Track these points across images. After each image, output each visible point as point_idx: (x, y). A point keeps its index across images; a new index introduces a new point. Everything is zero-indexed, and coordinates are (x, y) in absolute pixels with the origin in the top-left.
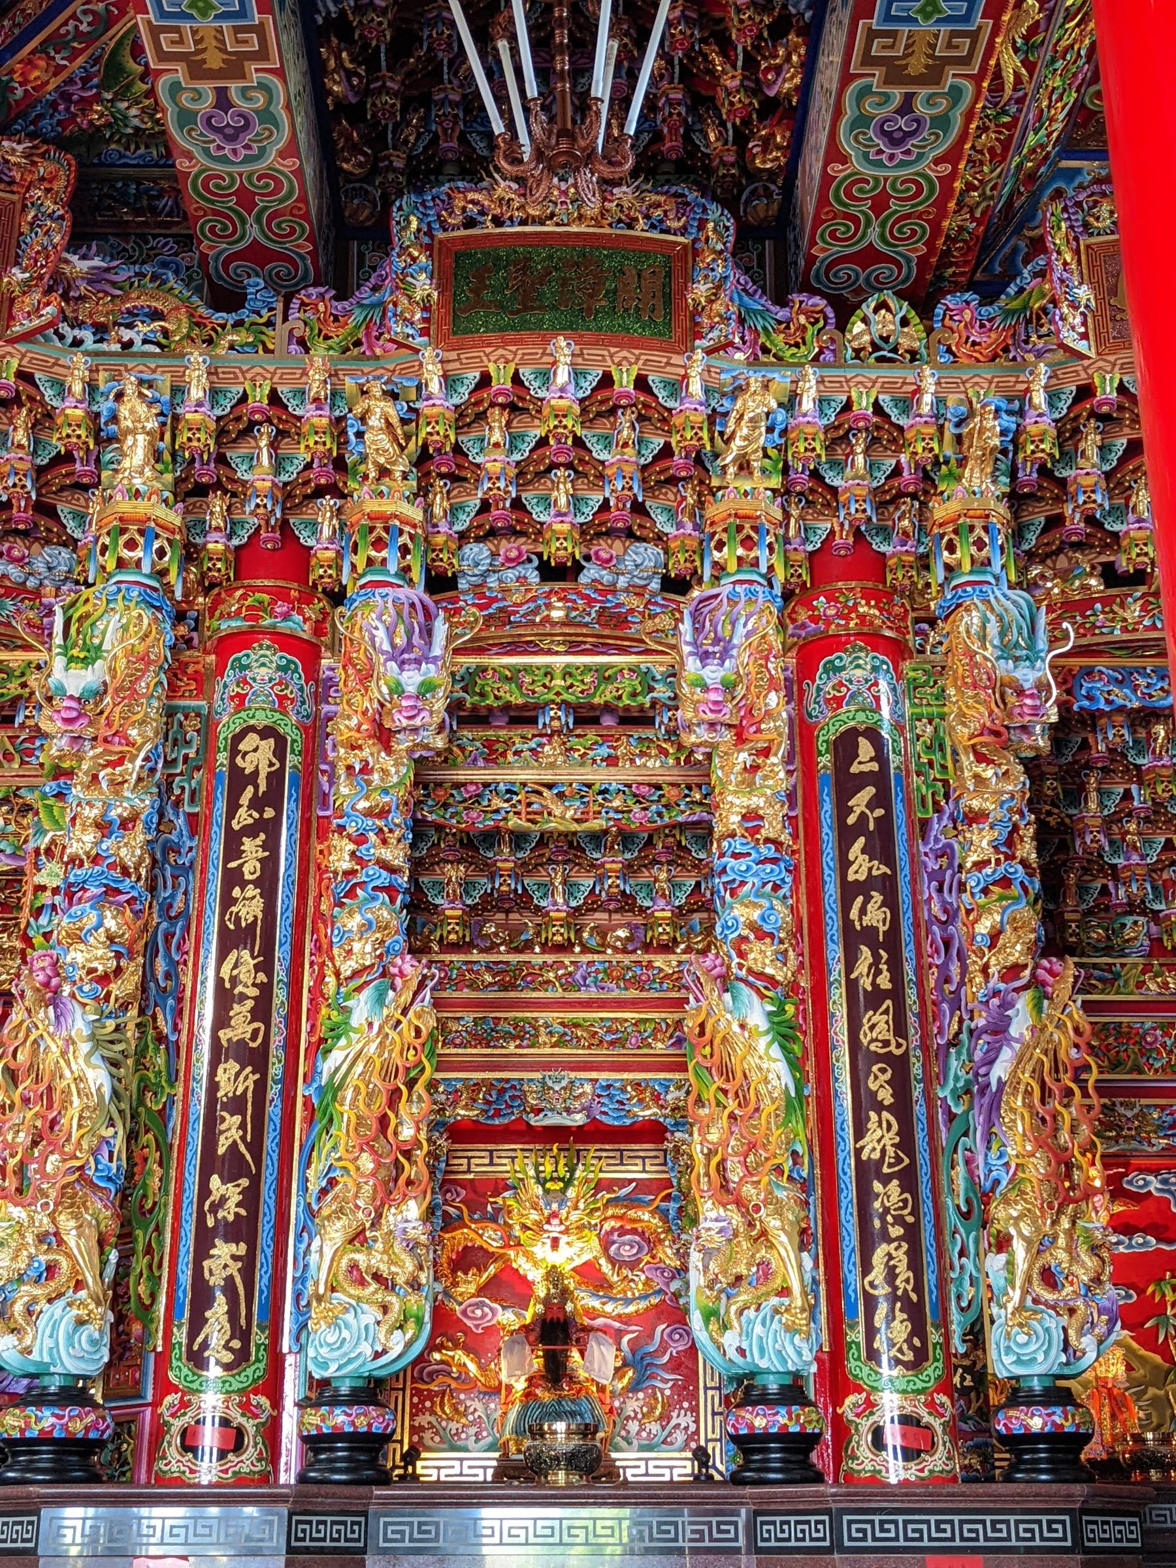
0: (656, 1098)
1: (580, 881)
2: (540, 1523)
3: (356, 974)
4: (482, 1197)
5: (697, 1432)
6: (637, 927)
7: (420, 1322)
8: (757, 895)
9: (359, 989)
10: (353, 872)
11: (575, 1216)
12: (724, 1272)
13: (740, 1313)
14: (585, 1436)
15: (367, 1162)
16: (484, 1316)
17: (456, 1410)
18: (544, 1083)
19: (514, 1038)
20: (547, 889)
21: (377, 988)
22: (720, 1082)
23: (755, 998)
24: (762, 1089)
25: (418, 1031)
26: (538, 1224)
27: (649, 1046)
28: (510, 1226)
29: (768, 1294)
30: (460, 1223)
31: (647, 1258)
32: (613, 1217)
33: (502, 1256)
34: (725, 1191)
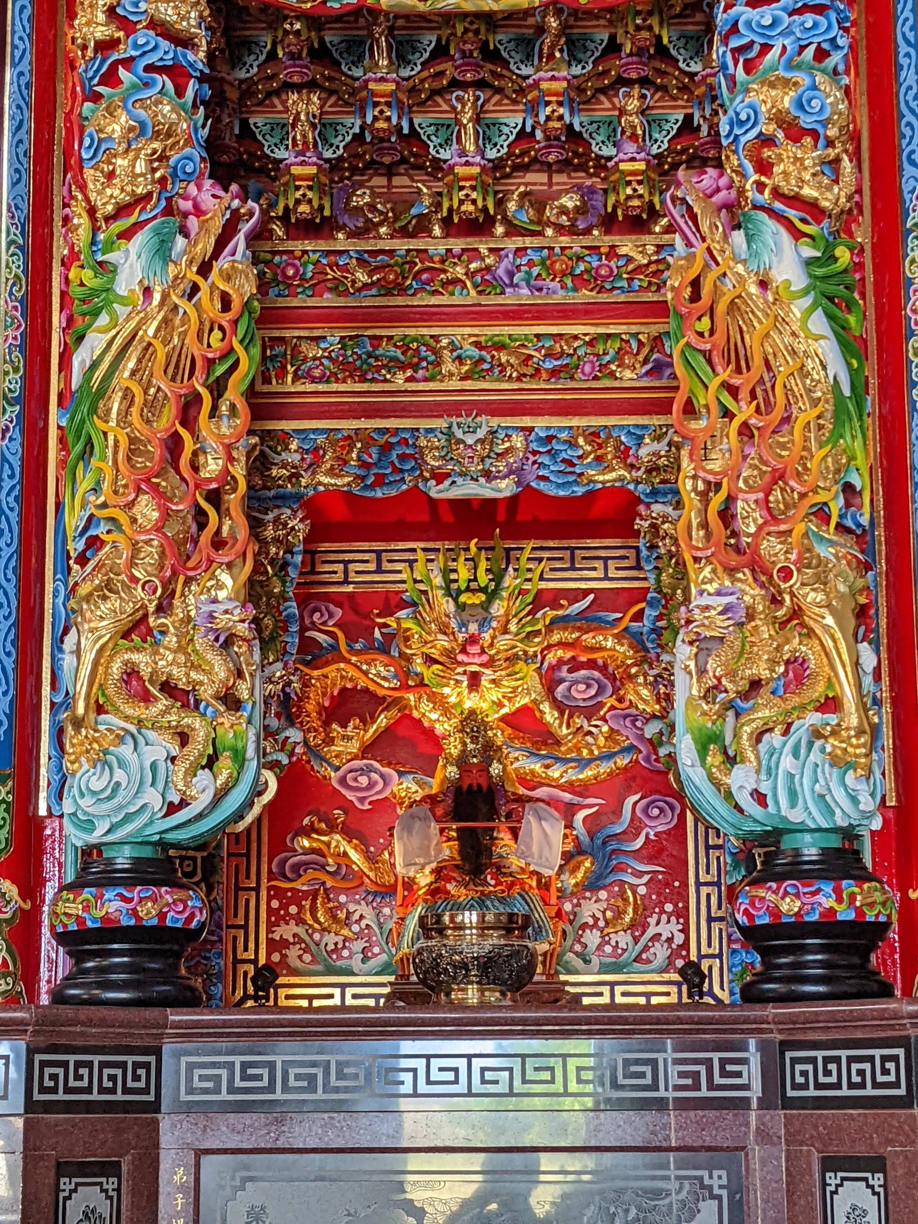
0: (623, 454)
1: (503, 118)
2: (435, 1063)
3: (122, 210)
4: (365, 617)
5: (686, 945)
6: (592, 190)
7: (239, 758)
8: (790, 66)
9: (127, 235)
10: (113, 44)
11: (503, 642)
12: (732, 674)
13: (758, 738)
14: (509, 931)
15: (147, 510)
16: (371, 785)
17: (334, 918)
18: (449, 433)
19: (403, 367)
20: (450, 131)
21: (157, 232)
22: (725, 374)
23: (785, 237)
24: (797, 386)
25: (226, 305)
26: (449, 653)
27: (612, 374)
28: (408, 659)
29: (803, 708)
30: (334, 654)
31: (612, 701)
32: (561, 644)
33: (396, 701)
34: (741, 557)
